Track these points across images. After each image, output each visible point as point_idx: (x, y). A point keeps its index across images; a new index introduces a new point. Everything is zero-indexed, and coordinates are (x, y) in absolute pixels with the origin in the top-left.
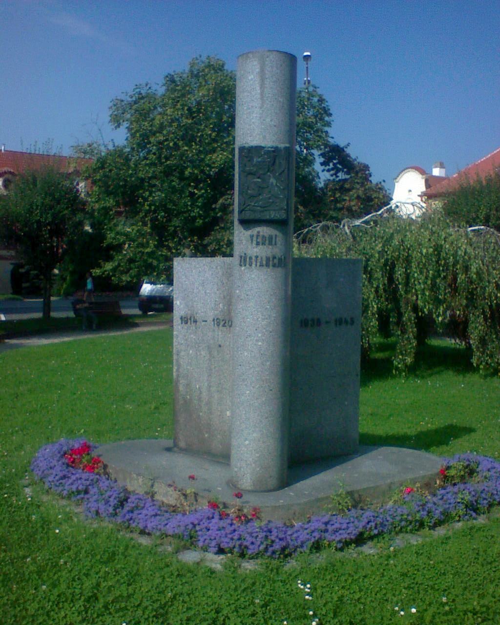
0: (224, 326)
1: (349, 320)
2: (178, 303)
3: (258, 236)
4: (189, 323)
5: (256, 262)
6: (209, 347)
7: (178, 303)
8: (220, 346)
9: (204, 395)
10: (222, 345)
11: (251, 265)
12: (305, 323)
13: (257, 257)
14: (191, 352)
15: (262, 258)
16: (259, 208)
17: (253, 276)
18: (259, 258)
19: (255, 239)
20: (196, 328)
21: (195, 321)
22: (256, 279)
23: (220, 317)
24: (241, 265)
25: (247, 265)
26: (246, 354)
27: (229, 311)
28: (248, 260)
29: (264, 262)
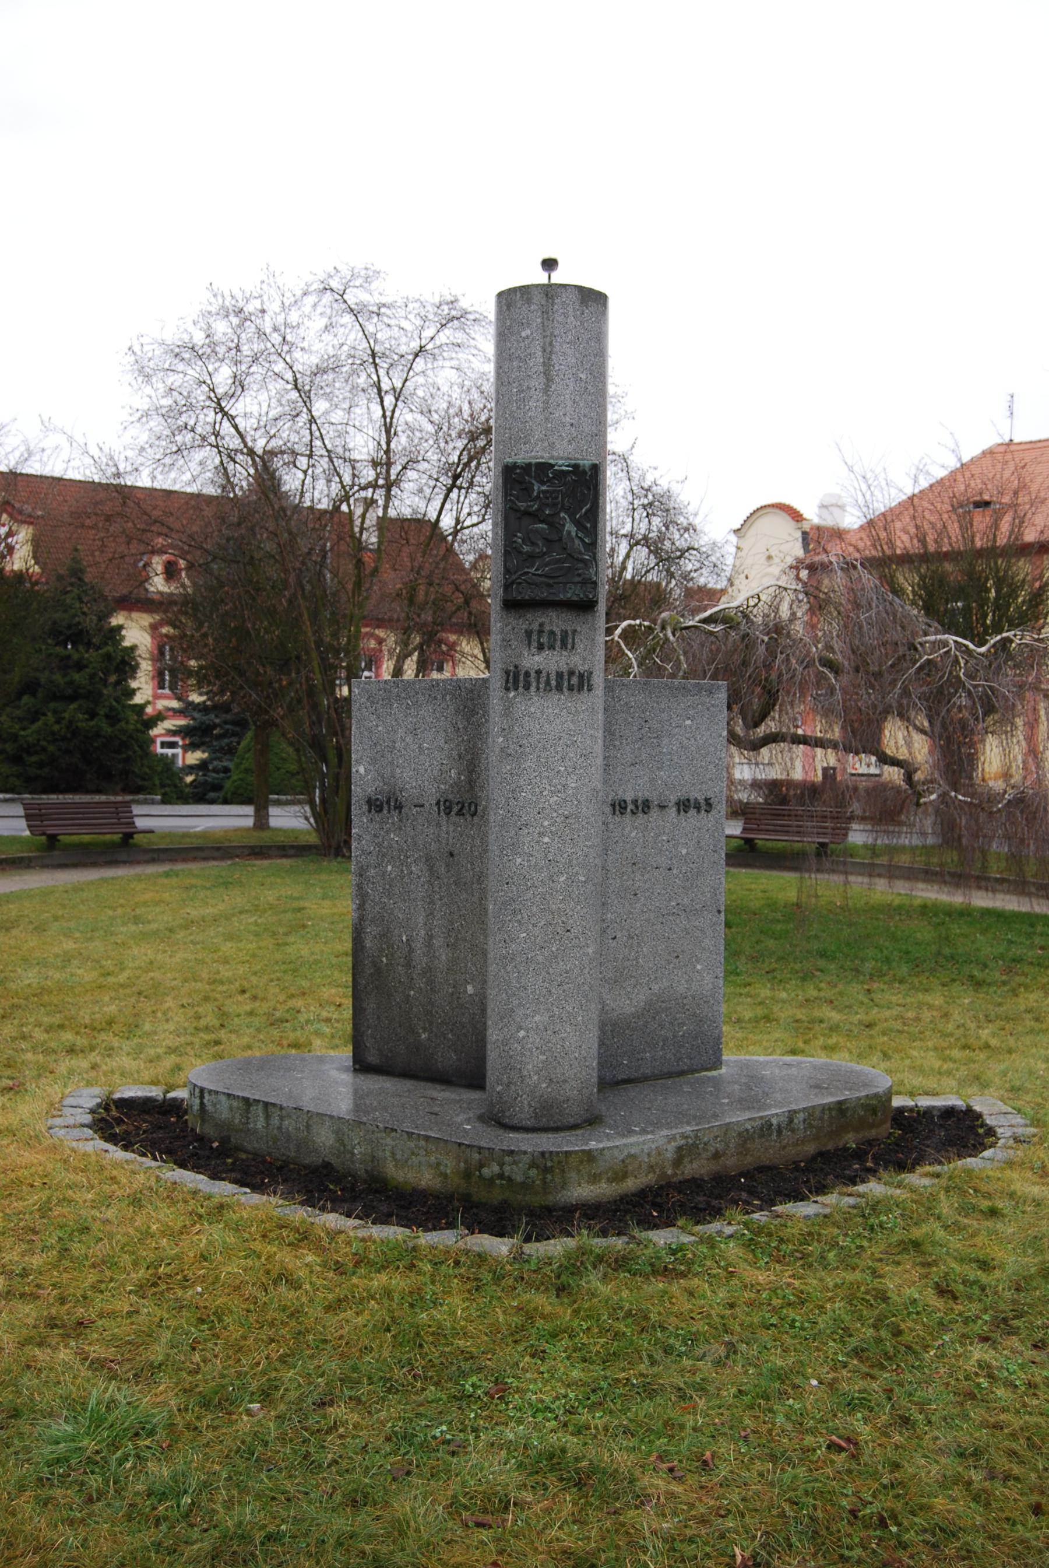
0: (460, 813)
1: (703, 802)
2: (362, 770)
3: (541, 632)
4: (385, 812)
5: (538, 682)
6: (428, 859)
7: (362, 770)
8: (452, 855)
9: (420, 958)
10: (456, 852)
11: (527, 687)
12: (619, 807)
13: (539, 672)
14: (389, 868)
15: (548, 674)
16: (543, 579)
17: (532, 710)
18: (544, 674)
19: (535, 637)
20: (401, 820)
21: (399, 807)
22: (539, 715)
23: (451, 797)
24: (507, 689)
25: (521, 689)
26: (519, 860)
27: (471, 783)
28: (521, 678)
29: (553, 683)
